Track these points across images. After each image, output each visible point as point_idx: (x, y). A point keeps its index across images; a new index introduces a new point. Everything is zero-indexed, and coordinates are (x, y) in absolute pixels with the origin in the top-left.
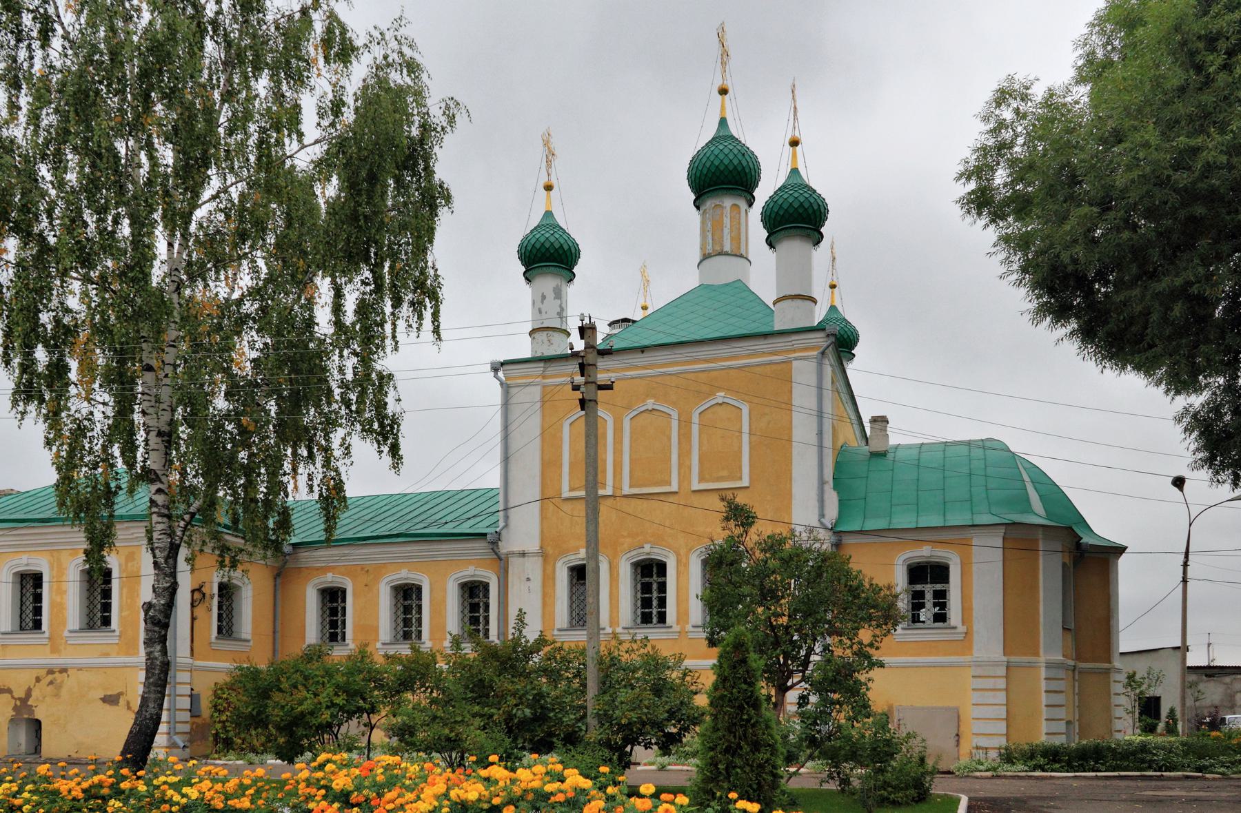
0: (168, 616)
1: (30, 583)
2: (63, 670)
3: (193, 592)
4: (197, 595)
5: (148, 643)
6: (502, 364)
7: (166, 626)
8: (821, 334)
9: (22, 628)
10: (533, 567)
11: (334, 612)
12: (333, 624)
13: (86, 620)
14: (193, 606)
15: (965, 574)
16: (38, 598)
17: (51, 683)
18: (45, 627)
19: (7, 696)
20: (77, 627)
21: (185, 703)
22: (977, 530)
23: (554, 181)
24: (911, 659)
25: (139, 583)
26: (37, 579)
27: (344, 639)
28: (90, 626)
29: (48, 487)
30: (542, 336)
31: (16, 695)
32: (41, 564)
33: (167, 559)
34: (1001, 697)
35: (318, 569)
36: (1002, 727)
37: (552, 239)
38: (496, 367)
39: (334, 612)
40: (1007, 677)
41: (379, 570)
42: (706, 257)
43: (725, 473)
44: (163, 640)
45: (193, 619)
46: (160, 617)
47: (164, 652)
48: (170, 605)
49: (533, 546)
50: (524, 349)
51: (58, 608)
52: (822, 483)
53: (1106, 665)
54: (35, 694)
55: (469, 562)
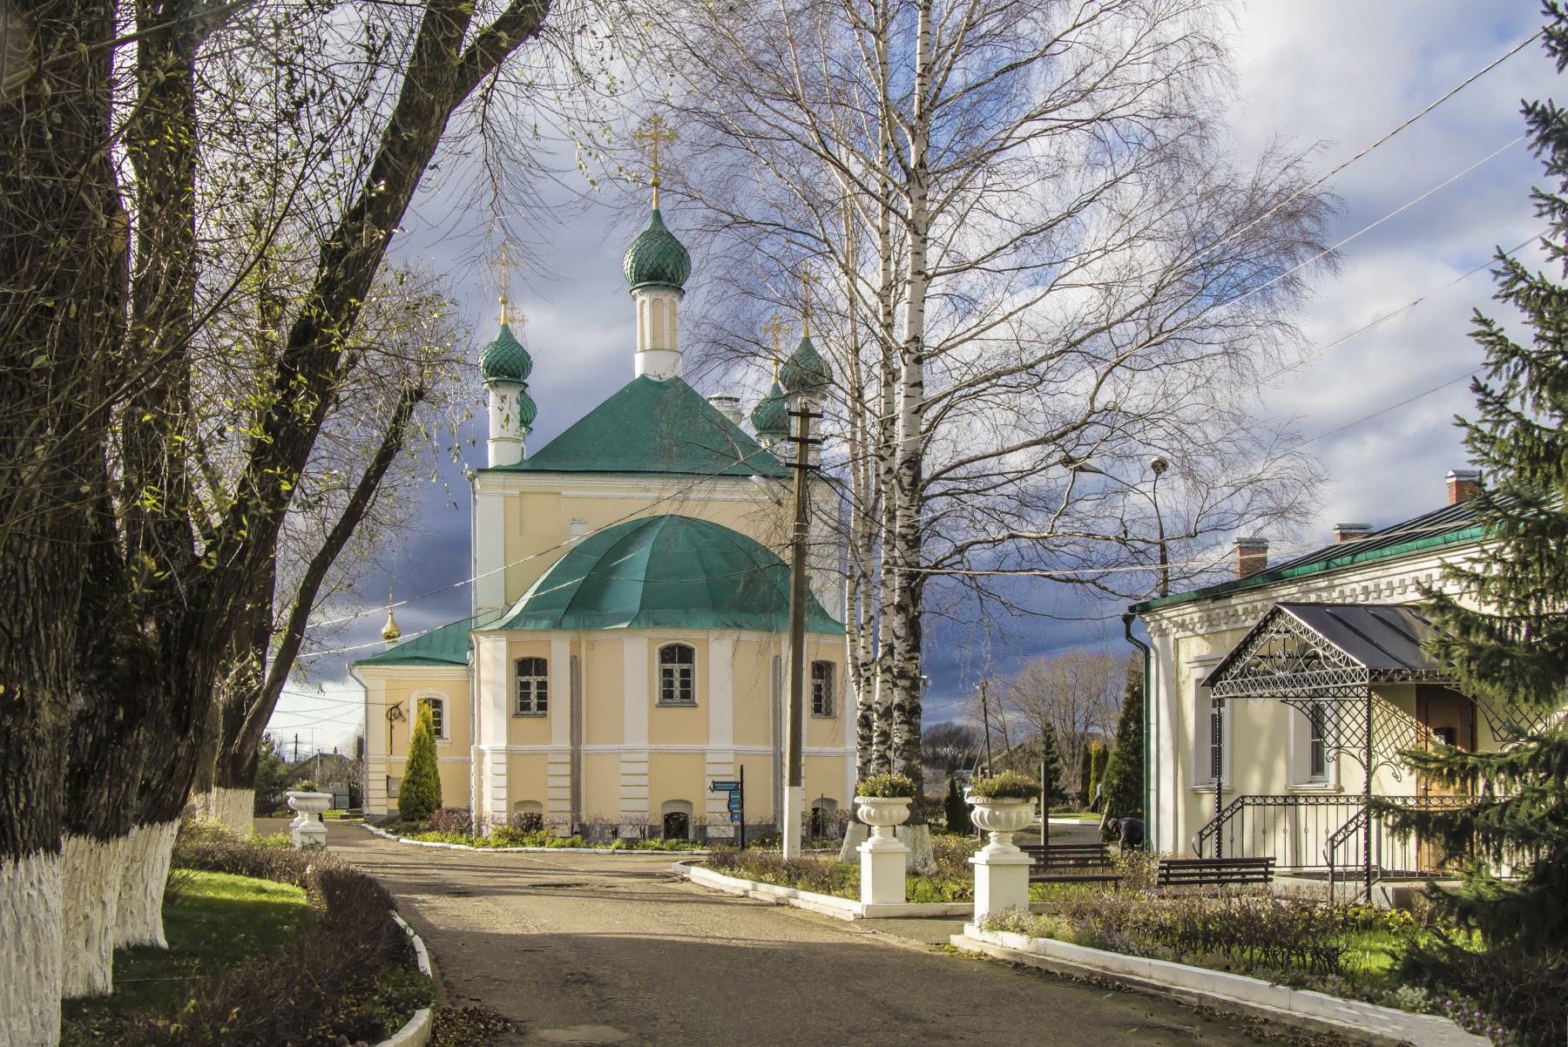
27: (543, 706)
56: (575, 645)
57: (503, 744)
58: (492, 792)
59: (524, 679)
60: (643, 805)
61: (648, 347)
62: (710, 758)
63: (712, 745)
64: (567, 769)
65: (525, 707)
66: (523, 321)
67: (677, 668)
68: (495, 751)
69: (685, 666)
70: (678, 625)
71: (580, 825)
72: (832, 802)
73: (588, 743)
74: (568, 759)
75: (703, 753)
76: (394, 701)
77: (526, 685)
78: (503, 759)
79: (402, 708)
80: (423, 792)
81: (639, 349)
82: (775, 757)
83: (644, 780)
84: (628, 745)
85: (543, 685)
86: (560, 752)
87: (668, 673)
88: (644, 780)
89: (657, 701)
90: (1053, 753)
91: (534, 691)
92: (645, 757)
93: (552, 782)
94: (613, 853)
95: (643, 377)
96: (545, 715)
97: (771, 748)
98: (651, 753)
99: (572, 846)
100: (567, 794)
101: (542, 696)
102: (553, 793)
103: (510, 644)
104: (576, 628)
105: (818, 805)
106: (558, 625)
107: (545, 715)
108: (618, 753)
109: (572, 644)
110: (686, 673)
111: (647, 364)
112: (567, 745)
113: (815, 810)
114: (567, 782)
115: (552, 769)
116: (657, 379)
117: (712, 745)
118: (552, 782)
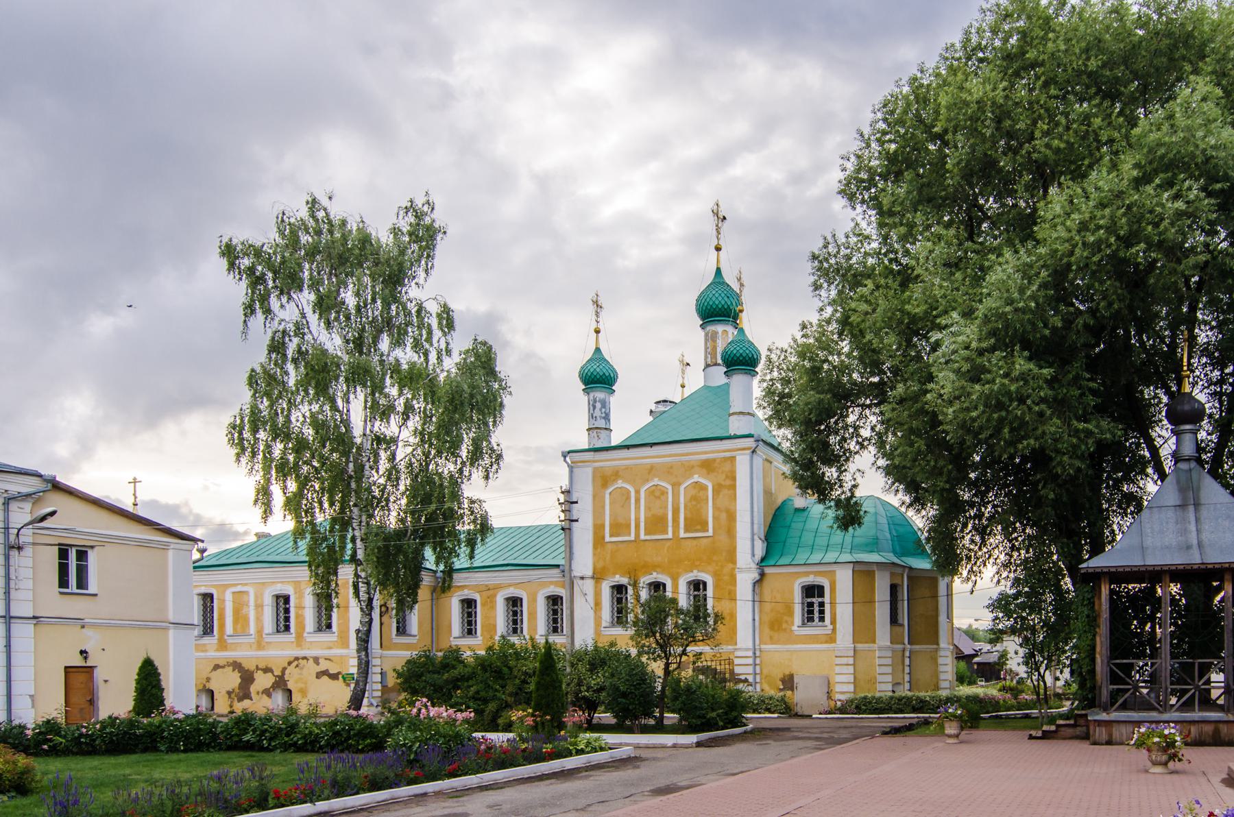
0: (368, 637)
1: (283, 601)
2: (304, 658)
3: (381, 606)
4: (384, 609)
5: (358, 651)
6: (569, 452)
7: (367, 642)
8: (752, 439)
9: (278, 631)
10: (589, 585)
11: (470, 615)
12: (470, 623)
13: (317, 625)
14: (381, 616)
15: (833, 590)
16: (287, 611)
17: (297, 666)
18: (292, 629)
19: (270, 674)
20: (312, 630)
21: (378, 678)
22: (840, 565)
23: (601, 326)
24: (804, 646)
25: (348, 611)
26: (287, 599)
27: (822, 619)
28: (319, 630)
29: (287, 533)
30: (594, 433)
31: (276, 674)
32: (289, 590)
33: (367, 606)
34: (851, 669)
35: (459, 587)
36: (851, 688)
37: (598, 370)
38: (565, 455)
39: (470, 615)
40: (854, 656)
41: (499, 587)
42: (707, 366)
43: (699, 527)
44: (366, 649)
45: (381, 624)
46: (364, 637)
47: (367, 655)
48: (369, 631)
49: (589, 572)
50: (582, 441)
51: (300, 618)
52: (753, 534)
53: (935, 646)
54: (287, 672)
55: (551, 583)
59: (809, 600)
85: (822, 605)
91: (816, 609)
101: (822, 612)
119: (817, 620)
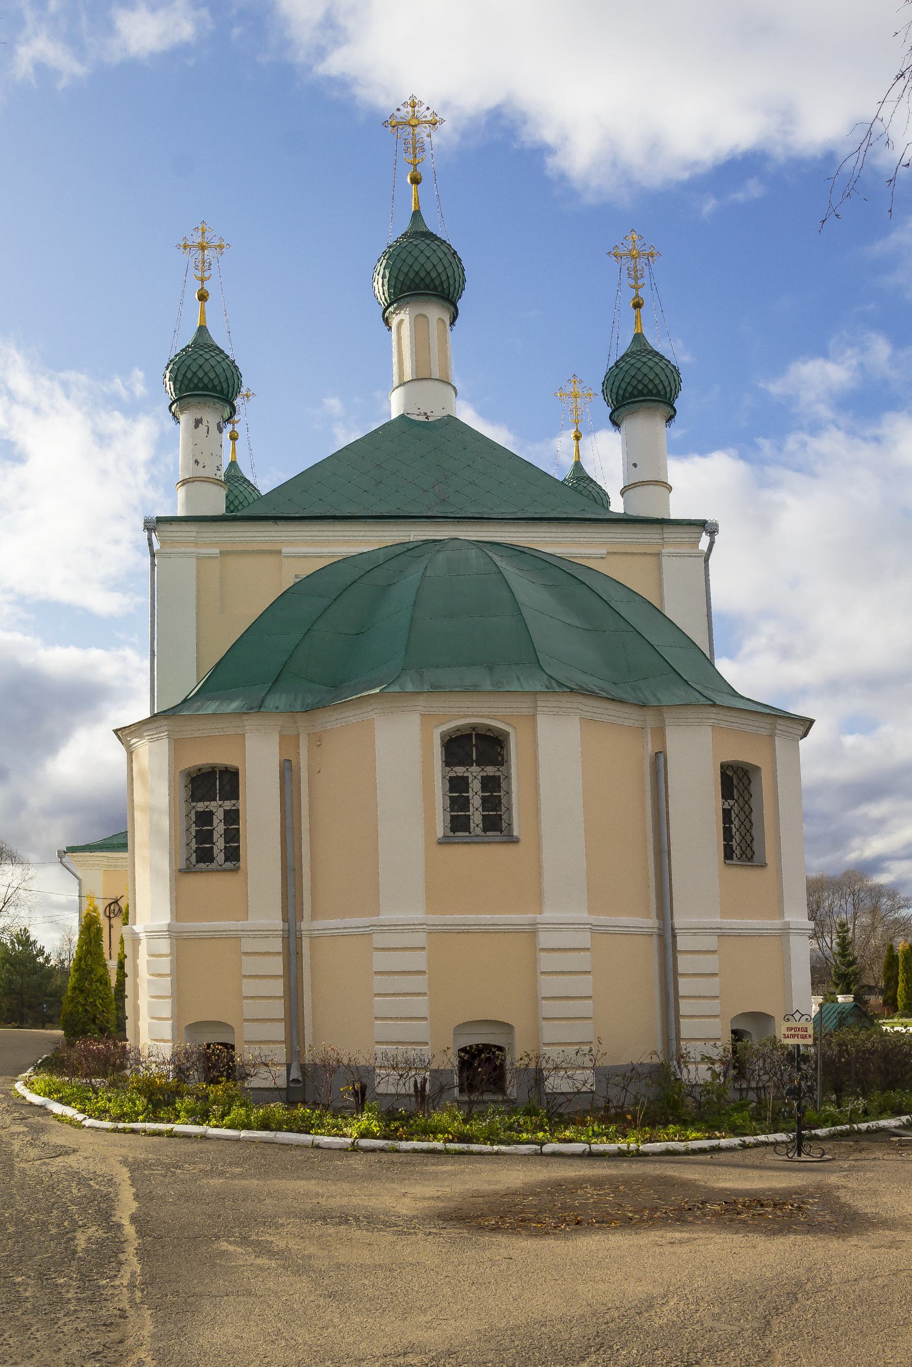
23: (207, 286)
27: (233, 855)
56: (288, 741)
57: (164, 920)
58: (151, 1007)
59: (201, 806)
60: (420, 1032)
61: (408, 376)
62: (546, 939)
63: (548, 915)
64: (276, 965)
65: (204, 856)
66: (221, 247)
67: (474, 774)
68: (153, 935)
69: (491, 771)
70: (473, 690)
71: (303, 1067)
72: (762, 1019)
73: (313, 917)
74: (277, 945)
75: (533, 931)
76: (114, 895)
77: (205, 818)
78: (164, 946)
79: (122, 903)
80: (93, 1004)
81: (396, 380)
82: (661, 936)
83: (420, 983)
84: (386, 917)
85: (232, 817)
86: (264, 934)
87: (457, 785)
88: (420, 983)
89: (440, 833)
90: (850, 955)
91: (219, 828)
92: (420, 939)
93: (250, 987)
94: (355, 1149)
95: (402, 417)
96: (236, 869)
97: (651, 922)
98: (433, 931)
99: (265, 1127)
100: (278, 1009)
101: (232, 836)
102: (251, 1009)
103: (177, 745)
104: (291, 712)
105: (739, 1026)
106: (257, 707)
107: (236, 869)
108: (366, 934)
109: (284, 739)
110: (492, 785)
111: (408, 399)
112: (277, 923)
113: (737, 1034)
114: (278, 987)
115: (250, 965)
116: (422, 418)
117: (548, 915)
118: (250, 987)
119: (220, 857)
